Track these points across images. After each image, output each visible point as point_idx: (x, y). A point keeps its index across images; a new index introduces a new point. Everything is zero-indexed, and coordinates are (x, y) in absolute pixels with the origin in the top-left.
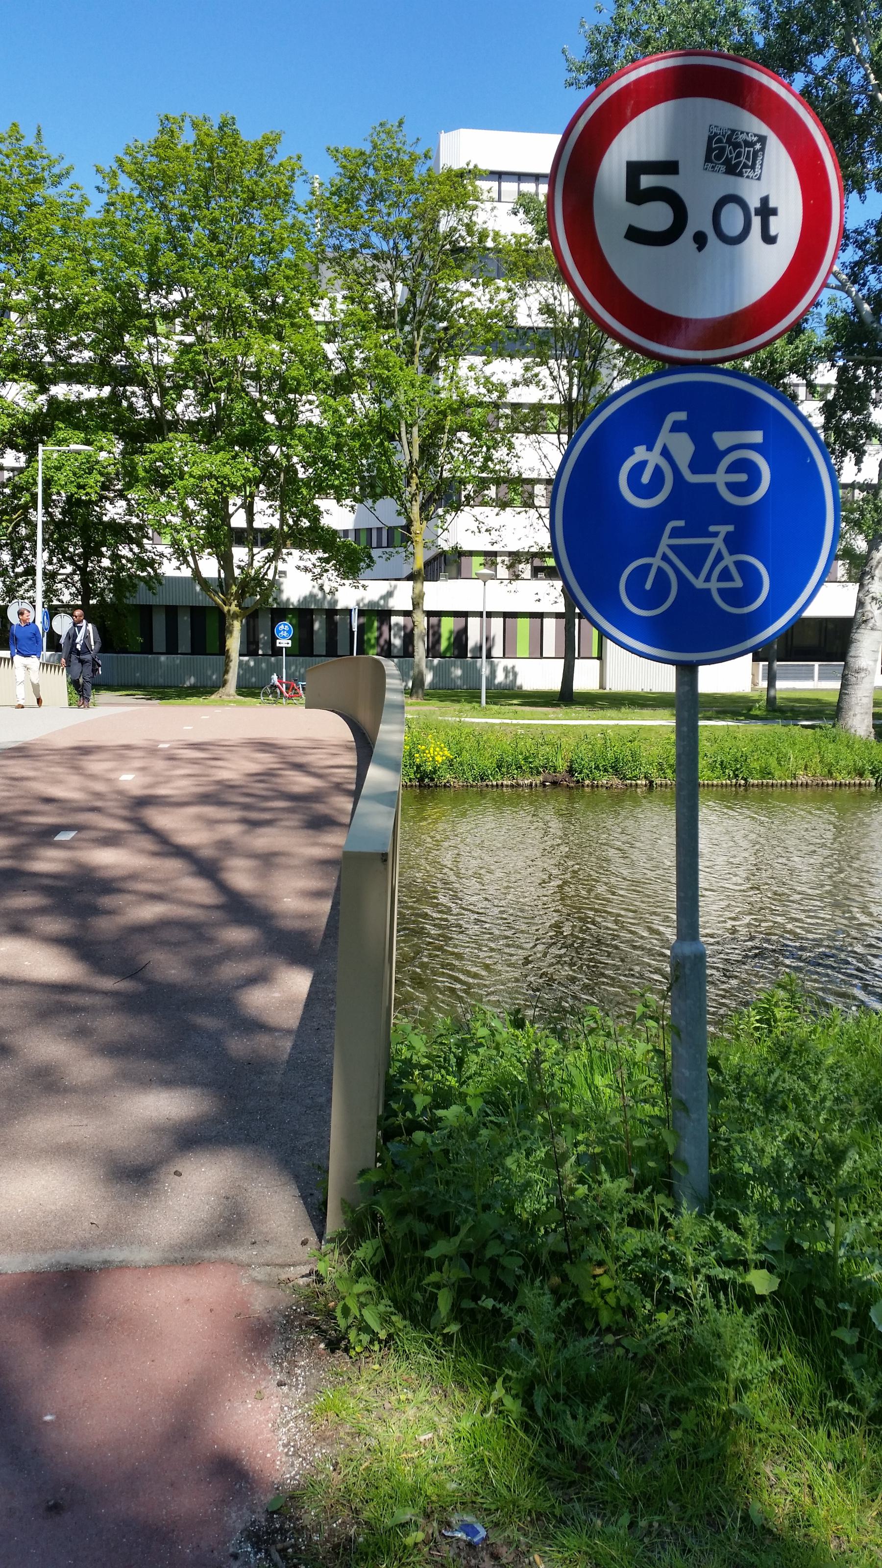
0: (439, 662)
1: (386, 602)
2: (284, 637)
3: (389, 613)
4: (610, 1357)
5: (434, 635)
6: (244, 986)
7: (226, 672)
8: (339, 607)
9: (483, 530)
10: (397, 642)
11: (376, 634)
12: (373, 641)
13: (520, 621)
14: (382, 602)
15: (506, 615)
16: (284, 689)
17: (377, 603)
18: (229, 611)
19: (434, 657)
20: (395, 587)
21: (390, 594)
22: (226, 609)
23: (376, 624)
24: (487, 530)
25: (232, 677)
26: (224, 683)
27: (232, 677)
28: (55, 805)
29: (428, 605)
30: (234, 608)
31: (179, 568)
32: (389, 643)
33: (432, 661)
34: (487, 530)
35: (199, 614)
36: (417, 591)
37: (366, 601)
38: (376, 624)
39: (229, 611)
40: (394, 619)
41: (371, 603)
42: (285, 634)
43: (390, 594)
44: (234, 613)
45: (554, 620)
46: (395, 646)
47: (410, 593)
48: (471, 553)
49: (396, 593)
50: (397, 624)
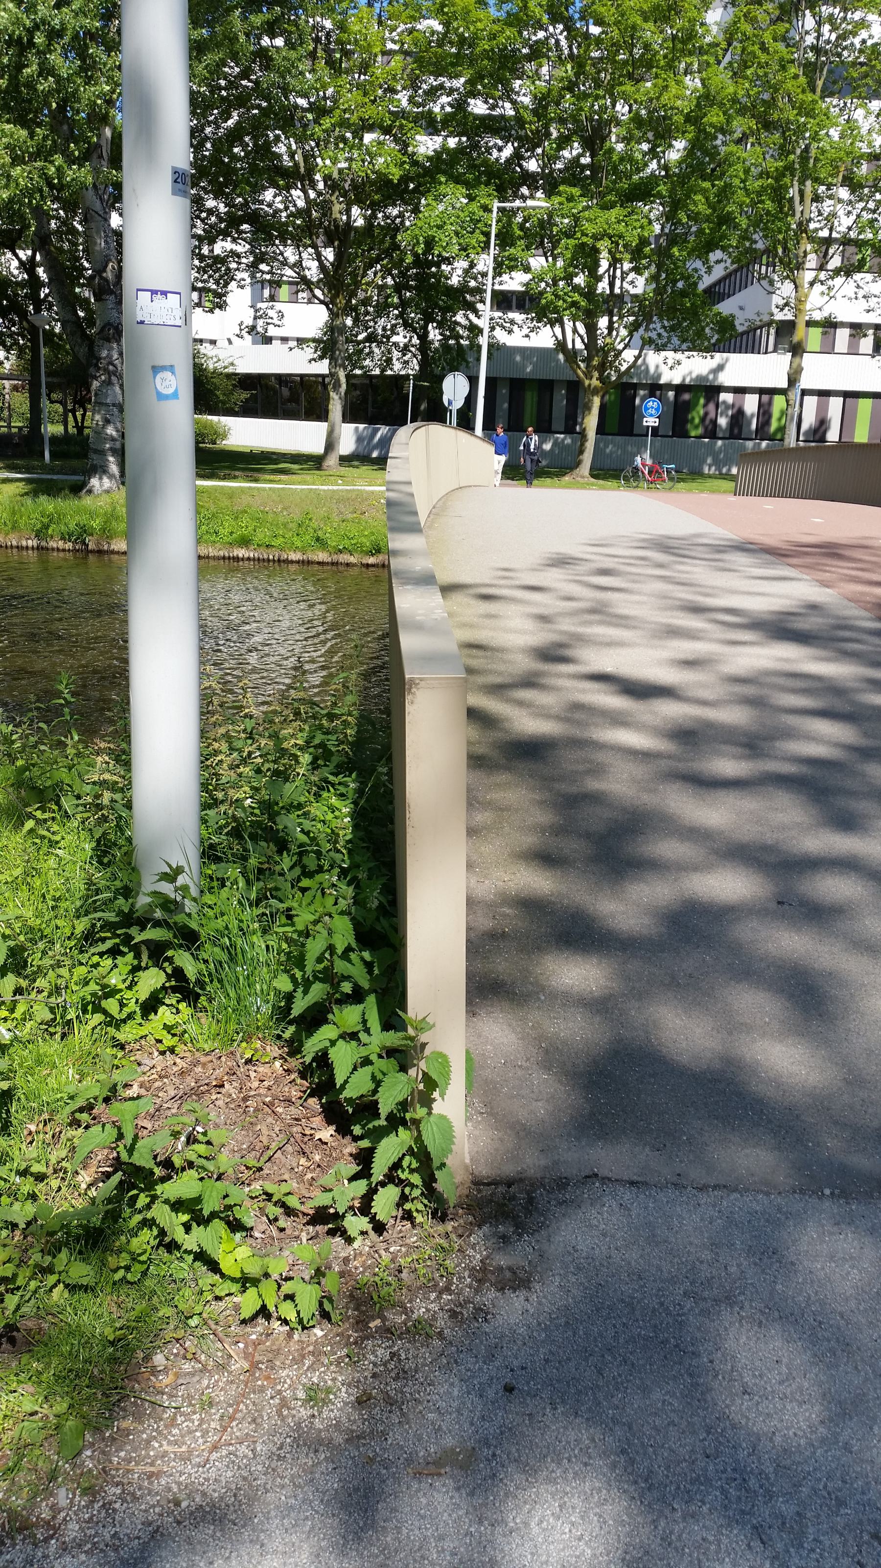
0: (768, 445)
1: (715, 378)
2: (651, 415)
3: (720, 389)
4: (232, 767)
5: (764, 414)
6: (725, 742)
7: (581, 452)
8: (662, 382)
9: (860, 296)
10: (723, 422)
11: (702, 412)
12: (697, 421)
13: (861, 401)
14: (711, 377)
15: (847, 395)
16: (646, 472)
17: (706, 378)
18: (590, 385)
19: (762, 439)
20: (727, 360)
21: (721, 368)
22: (587, 382)
23: (702, 401)
24: (864, 297)
25: (587, 458)
26: (578, 464)
27: (587, 458)
28: (562, 594)
29: (805, 382)
30: (595, 382)
31: (527, 336)
32: (714, 422)
33: (759, 444)
34: (864, 297)
35: (546, 387)
36: (795, 365)
37: (694, 375)
38: (702, 401)
39: (590, 385)
40: (723, 396)
41: (699, 378)
42: (653, 412)
43: (721, 368)
44: (595, 387)
45: (815, 398)
46: (720, 426)
47: (786, 368)
48: (843, 325)
49: (728, 366)
50: (724, 402)
